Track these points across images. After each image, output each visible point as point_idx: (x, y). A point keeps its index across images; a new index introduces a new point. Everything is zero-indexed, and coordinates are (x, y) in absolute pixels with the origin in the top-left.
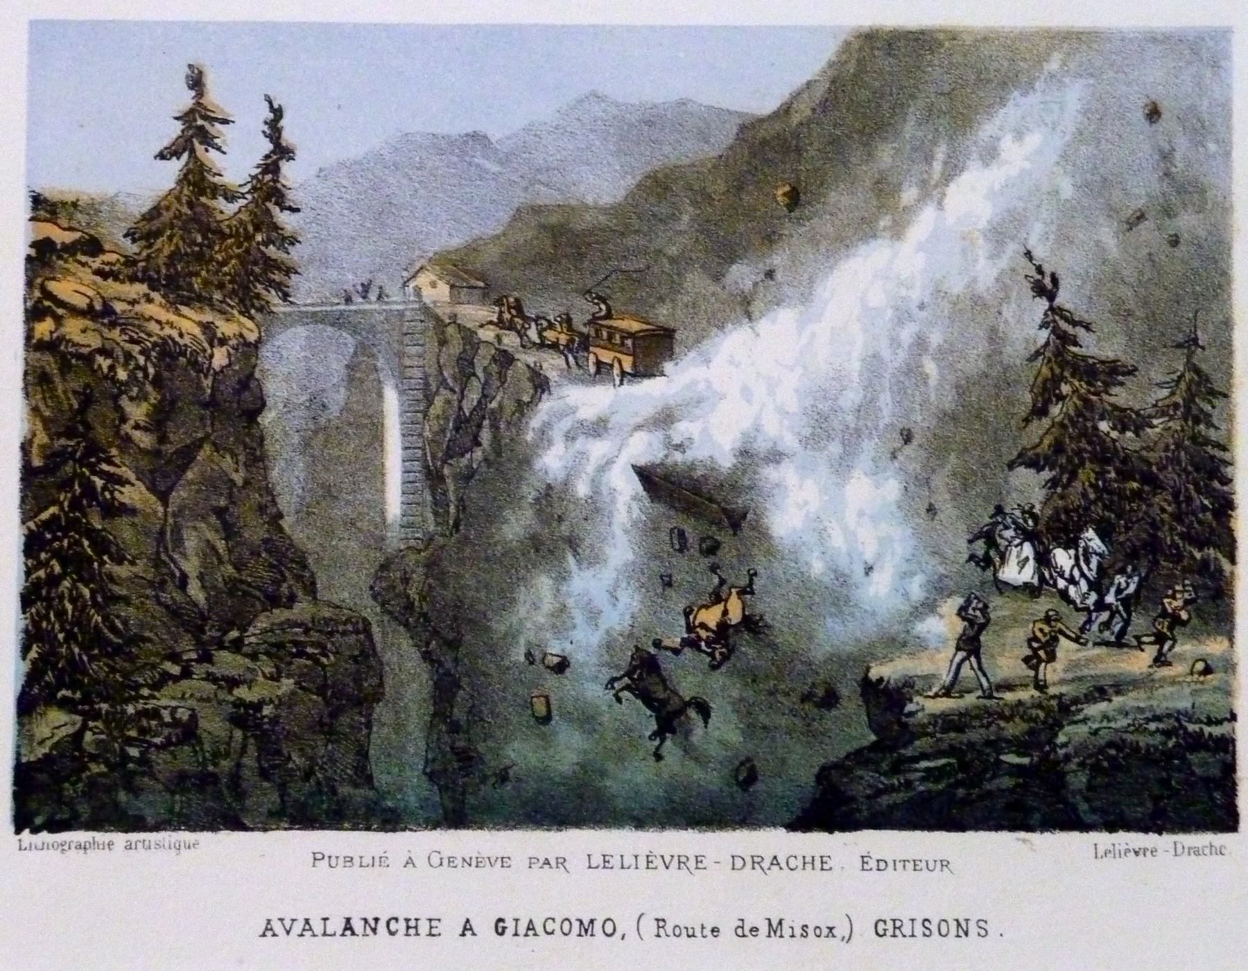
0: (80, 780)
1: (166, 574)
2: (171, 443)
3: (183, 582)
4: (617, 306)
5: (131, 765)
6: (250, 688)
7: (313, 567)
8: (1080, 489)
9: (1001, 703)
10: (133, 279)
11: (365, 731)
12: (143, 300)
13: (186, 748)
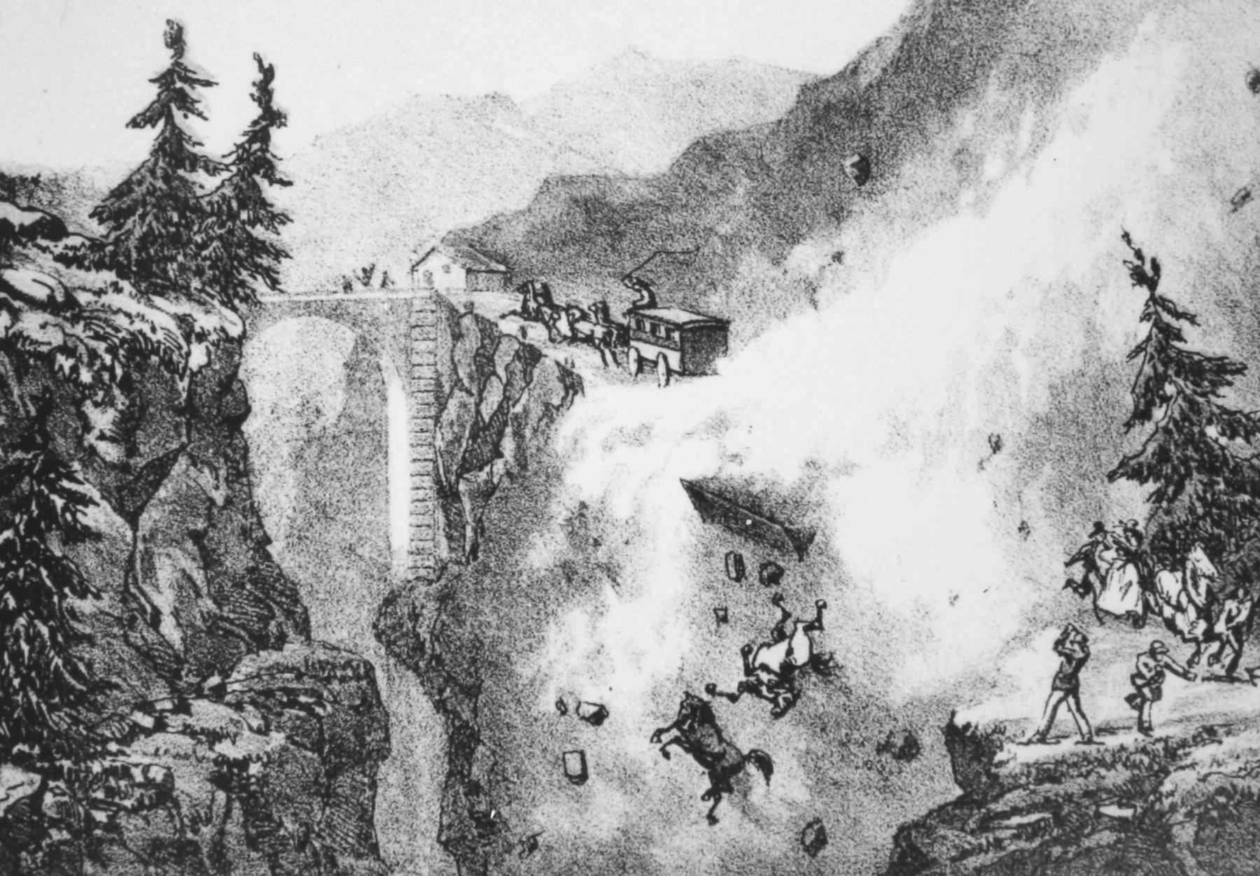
0: (39, 848)
1: (136, 609)
2: (141, 455)
3: (155, 620)
4: (662, 293)
5: (98, 832)
6: (234, 743)
7: (306, 600)
8: (1187, 503)
9: (1102, 748)
10: (99, 266)
11: (368, 793)
12: (110, 290)
13: (160, 811)
